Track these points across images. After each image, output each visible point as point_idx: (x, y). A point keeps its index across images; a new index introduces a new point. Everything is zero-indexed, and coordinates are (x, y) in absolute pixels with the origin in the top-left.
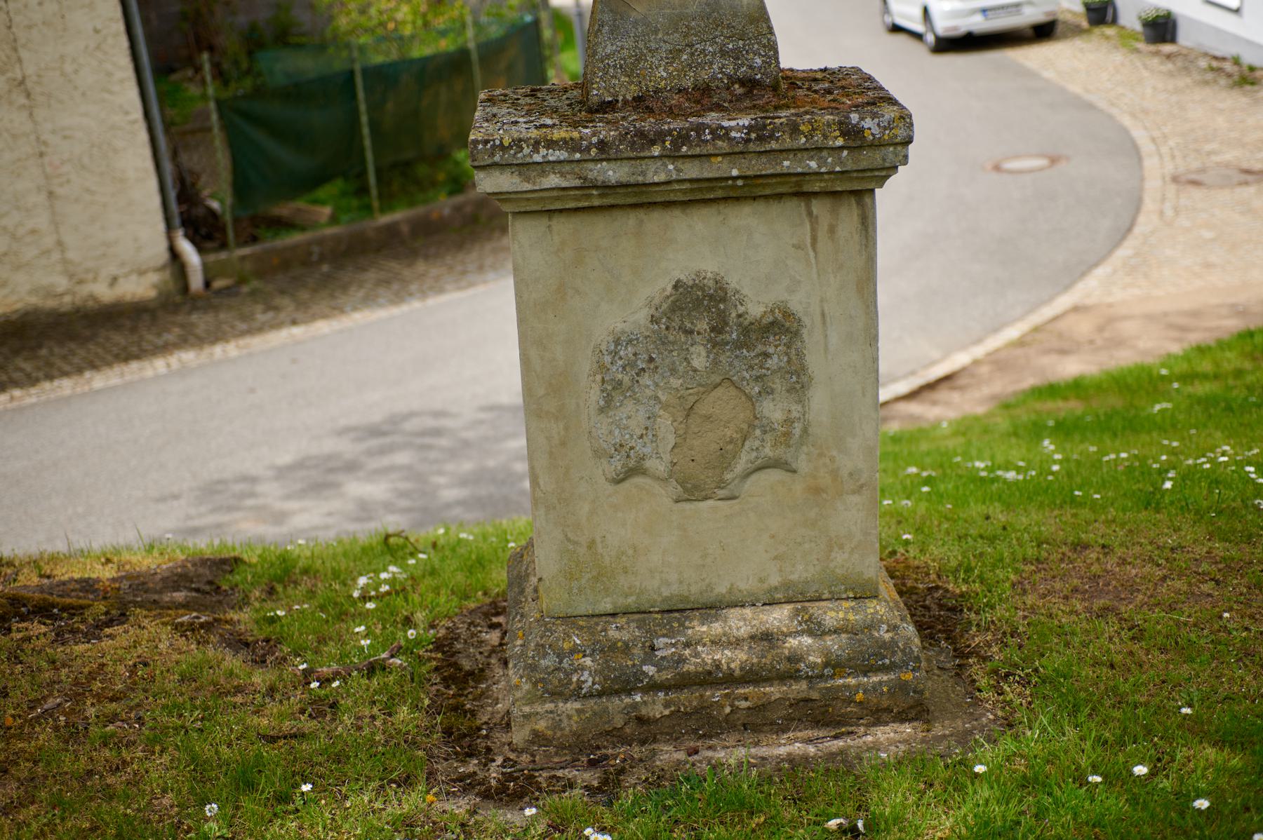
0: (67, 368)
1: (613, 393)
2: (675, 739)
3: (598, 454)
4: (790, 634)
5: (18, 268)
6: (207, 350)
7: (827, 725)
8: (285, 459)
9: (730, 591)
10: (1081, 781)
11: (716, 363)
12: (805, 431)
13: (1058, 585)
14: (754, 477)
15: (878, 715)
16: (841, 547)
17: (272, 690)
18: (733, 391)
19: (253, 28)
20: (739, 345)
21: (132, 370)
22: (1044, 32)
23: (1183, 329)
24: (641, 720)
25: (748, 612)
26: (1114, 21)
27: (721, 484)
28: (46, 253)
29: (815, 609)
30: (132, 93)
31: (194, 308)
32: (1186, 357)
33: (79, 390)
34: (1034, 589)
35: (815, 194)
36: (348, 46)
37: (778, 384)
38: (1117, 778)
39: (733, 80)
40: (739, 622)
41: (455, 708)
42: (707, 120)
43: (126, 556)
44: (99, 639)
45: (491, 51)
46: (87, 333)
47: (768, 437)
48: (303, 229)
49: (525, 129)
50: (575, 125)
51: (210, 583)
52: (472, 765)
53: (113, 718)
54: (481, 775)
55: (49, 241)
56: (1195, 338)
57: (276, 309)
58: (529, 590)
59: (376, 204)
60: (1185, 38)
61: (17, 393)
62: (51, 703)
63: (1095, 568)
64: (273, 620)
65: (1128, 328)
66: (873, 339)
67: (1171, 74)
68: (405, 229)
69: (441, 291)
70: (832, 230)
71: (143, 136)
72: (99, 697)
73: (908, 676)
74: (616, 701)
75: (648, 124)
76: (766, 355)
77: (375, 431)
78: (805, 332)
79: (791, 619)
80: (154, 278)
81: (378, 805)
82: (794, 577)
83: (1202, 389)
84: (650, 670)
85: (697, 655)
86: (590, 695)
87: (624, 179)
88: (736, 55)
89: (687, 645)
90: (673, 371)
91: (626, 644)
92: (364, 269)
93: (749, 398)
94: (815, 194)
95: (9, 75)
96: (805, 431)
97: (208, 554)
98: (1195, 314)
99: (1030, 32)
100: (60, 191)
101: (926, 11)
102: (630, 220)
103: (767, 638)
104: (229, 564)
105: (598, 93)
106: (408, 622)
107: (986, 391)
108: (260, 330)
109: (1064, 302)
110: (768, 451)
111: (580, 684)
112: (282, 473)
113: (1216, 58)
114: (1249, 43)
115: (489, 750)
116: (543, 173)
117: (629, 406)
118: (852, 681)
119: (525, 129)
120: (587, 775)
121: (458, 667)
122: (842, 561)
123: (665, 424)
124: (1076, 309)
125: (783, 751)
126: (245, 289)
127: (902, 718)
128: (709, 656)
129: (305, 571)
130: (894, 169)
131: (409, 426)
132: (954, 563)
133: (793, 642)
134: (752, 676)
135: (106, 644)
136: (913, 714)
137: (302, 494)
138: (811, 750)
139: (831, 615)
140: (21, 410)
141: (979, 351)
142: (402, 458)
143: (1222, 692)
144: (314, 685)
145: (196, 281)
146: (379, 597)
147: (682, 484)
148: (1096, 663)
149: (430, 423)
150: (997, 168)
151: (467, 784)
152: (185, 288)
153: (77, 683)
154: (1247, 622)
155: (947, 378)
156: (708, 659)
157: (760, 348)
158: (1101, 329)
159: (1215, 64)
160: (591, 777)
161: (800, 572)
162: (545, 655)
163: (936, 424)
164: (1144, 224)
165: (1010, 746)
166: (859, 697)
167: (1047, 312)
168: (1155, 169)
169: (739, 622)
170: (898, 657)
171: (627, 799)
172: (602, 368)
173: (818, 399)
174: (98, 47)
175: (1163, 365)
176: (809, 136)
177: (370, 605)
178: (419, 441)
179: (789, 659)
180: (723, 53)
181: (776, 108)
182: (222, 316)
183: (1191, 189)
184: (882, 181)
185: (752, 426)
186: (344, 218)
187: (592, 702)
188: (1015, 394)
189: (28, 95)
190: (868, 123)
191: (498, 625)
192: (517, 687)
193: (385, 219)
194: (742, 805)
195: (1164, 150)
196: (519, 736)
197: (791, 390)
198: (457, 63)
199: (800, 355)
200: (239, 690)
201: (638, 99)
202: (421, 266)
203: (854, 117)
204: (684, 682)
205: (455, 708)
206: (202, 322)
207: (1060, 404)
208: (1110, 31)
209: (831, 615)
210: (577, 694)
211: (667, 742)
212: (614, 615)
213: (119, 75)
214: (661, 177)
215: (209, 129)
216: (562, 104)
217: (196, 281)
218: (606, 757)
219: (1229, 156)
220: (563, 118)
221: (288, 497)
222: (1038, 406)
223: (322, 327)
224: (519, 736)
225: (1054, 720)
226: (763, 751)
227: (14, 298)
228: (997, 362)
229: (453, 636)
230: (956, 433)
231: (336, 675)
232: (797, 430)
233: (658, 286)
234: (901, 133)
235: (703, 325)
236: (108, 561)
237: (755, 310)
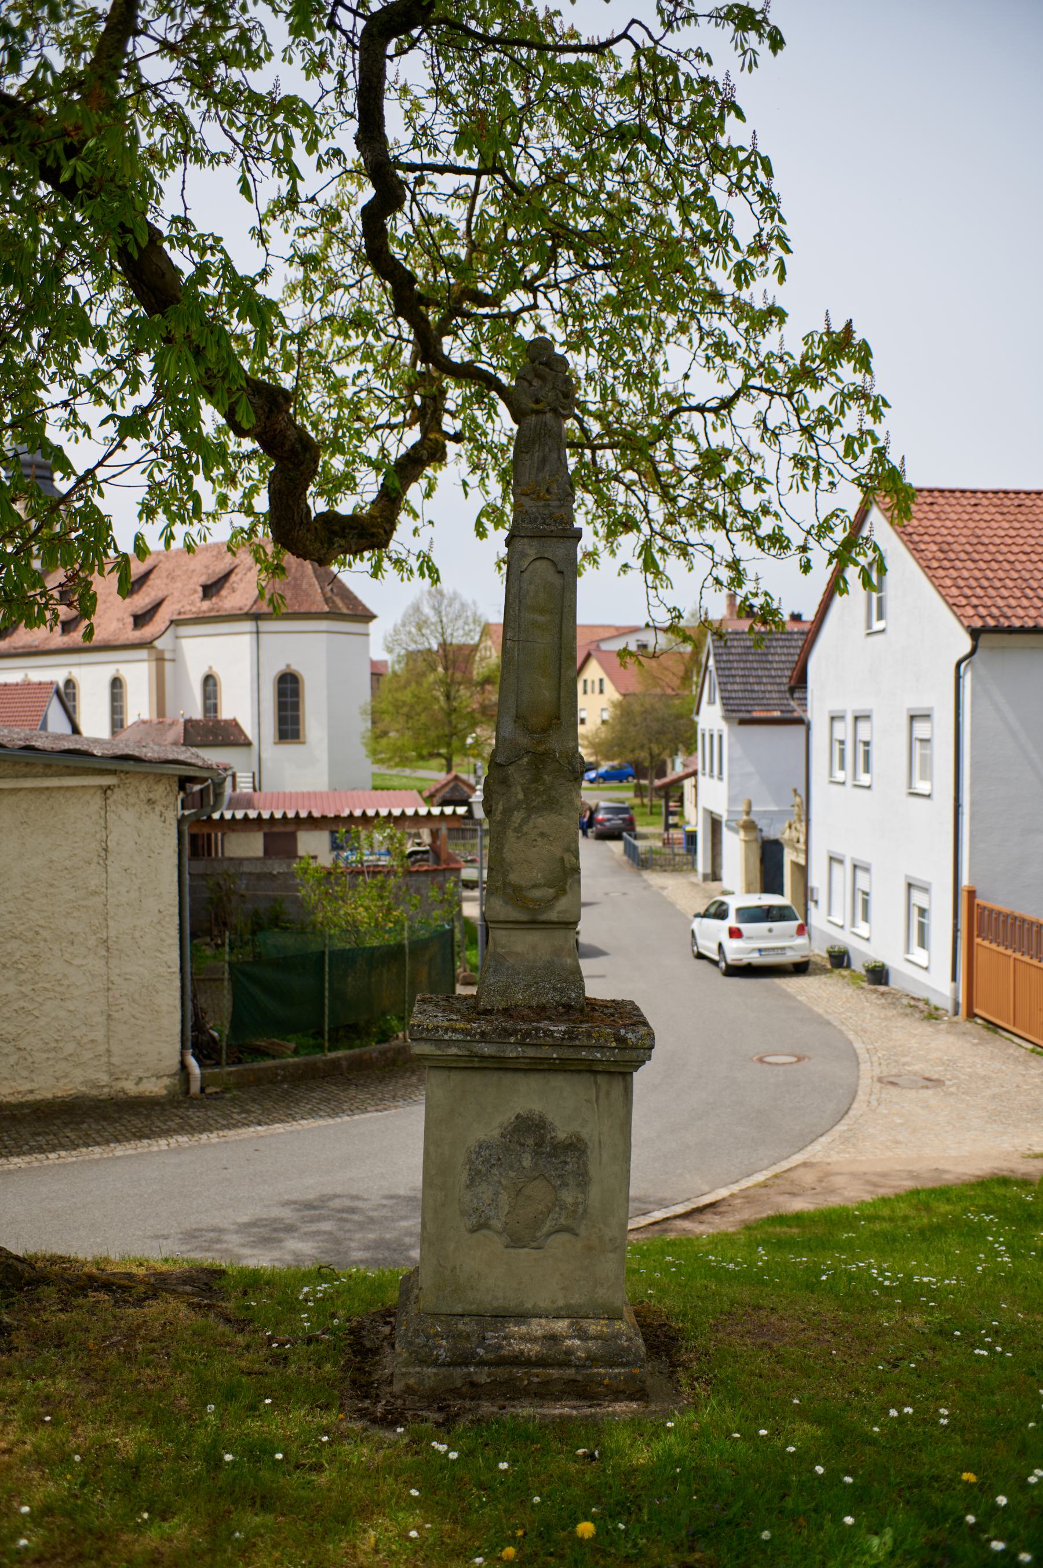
0: (99, 1139)
1: (475, 1177)
2: (492, 1399)
3: (463, 1213)
4: (567, 1337)
5: (77, 1065)
6: (197, 1137)
7: (585, 1398)
8: (245, 1219)
9: (534, 1307)
10: (728, 1435)
11: (536, 1164)
12: (585, 1210)
13: (739, 1328)
14: (553, 1237)
15: (617, 1395)
16: (602, 1285)
17: (248, 1347)
18: (545, 1183)
19: (256, 913)
20: (550, 1155)
21: (144, 1146)
22: (800, 969)
23: (876, 1185)
24: (473, 1384)
25: (543, 1321)
26: (848, 966)
27: (534, 1239)
28: (98, 1057)
29: (584, 1323)
30: (175, 954)
31: (192, 1106)
32: (873, 1205)
33: (105, 1156)
34: (724, 1327)
35: (599, 1072)
36: (322, 934)
37: (571, 1181)
38: (750, 1437)
39: (559, 1004)
40: (537, 1327)
41: (359, 1369)
42: (542, 1025)
43: (152, 1263)
44: (142, 1307)
45: (419, 947)
46: (116, 1115)
47: (563, 1212)
48: (274, 1057)
49: (441, 1021)
50: (469, 1021)
51: (206, 1284)
52: (367, 1403)
53: (153, 1351)
54: (371, 1409)
55: (102, 1049)
56: (882, 1192)
57: (248, 1112)
58: (412, 1297)
59: (327, 1045)
60: (894, 982)
61: (63, 1153)
62: (115, 1339)
63: (764, 1321)
64: (248, 1308)
65: (839, 1181)
66: (627, 1159)
67: (883, 1007)
68: (344, 1063)
69: (365, 1111)
70: (608, 1093)
71: (177, 983)
72: (144, 1339)
73: (637, 1371)
74: (458, 1370)
75: (508, 1025)
76: (566, 1163)
77: (309, 1206)
78: (589, 1151)
79: (569, 1327)
80: (166, 1081)
81: (309, 1418)
82: (573, 1302)
83: (877, 1227)
84: (481, 1351)
85: (510, 1345)
86: (443, 1365)
87: (493, 1054)
88: (562, 991)
89: (505, 1338)
90: (511, 1167)
91: (468, 1334)
92: (312, 1090)
93: (554, 1187)
94: (599, 1072)
96: (585, 1210)
97: (205, 1265)
98: (884, 1175)
99: (791, 968)
100: (115, 1015)
101: (720, 946)
102: (495, 1076)
103: (553, 1338)
104: (219, 1273)
105: (483, 1004)
106: (333, 1316)
107: (738, 1217)
108: (235, 1126)
109: (797, 1159)
110: (563, 1221)
111: (438, 1355)
112: (243, 1228)
113: (913, 998)
114: (935, 991)
115: (378, 1395)
116: (449, 1046)
117: (484, 1186)
118: (602, 1370)
119: (441, 1021)
120: (436, 1416)
121: (363, 1346)
122: (602, 1294)
123: (504, 1197)
124: (805, 1164)
125: (557, 1412)
126: (228, 1096)
127: (631, 1398)
128: (517, 1346)
129: (267, 1283)
130: (643, 1062)
131: (336, 1203)
132: (677, 1310)
133: (569, 1342)
134: (541, 1362)
135: (146, 1310)
136: (638, 1396)
137: (253, 1245)
138: (575, 1412)
139: (593, 1327)
140: (64, 1165)
141: (735, 1188)
142: (326, 1226)
143: (822, 1395)
144: (275, 1345)
146: (316, 1300)
147: (510, 1236)
148: (752, 1374)
149: (348, 1203)
150: (761, 1060)
151: (363, 1414)
152: (187, 1091)
153: (130, 1329)
154: (846, 1358)
155: (712, 1205)
156: (517, 1348)
157: (562, 1158)
158: (820, 1181)
159: (912, 1003)
160: (439, 1417)
161: (576, 1299)
162: (418, 1337)
163: (698, 1237)
164: (858, 1108)
165: (692, 1416)
166: (606, 1381)
167: (785, 1165)
168: (867, 1072)
169: (537, 1327)
170: (631, 1358)
171: (460, 1427)
172: (470, 1161)
173: (595, 1192)
175: (857, 1209)
176: (598, 1040)
177: (311, 1304)
178: (339, 1215)
179: (565, 1353)
180: (555, 989)
181: (581, 1022)
182: (210, 1114)
183: (889, 1087)
184: (636, 1068)
185: (554, 1205)
186: (302, 1052)
187: (443, 1369)
188: (756, 1221)
189: (108, 950)
190: (630, 1035)
191: (390, 1323)
192: (400, 1354)
193: (332, 1055)
194: (528, 1438)
195: (875, 1059)
196: (397, 1387)
197: (578, 1185)
198: (394, 954)
199: (585, 1165)
200: (228, 1344)
201: (506, 1010)
202: (352, 1092)
203: (623, 1032)
204: (501, 1362)
205: (359, 1369)
206: (195, 1115)
207: (785, 1229)
208: (845, 972)
209: (593, 1327)
210: (435, 1363)
211: (487, 1400)
212: (462, 1316)
213: (169, 941)
214: (514, 1055)
215: (222, 980)
216: (462, 1007)
218: (449, 1406)
219: (917, 1067)
220: (463, 1016)
221: (243, 1245)
222: (770, 1230)
223: (278, 1128)
224: (397, 1387)
225: (720, 1404)
226: (545, 1411)
227: (71, 1086)
228: (748, 1197)
229: (361, 1327)
230: (710, 1243)
231: (288, 1341)
232: (580, 1210)
233: (506, 1116)
234: (647, 1043)
235: (530, 1142)
236: (141, 1264)
237: (562, 1136)
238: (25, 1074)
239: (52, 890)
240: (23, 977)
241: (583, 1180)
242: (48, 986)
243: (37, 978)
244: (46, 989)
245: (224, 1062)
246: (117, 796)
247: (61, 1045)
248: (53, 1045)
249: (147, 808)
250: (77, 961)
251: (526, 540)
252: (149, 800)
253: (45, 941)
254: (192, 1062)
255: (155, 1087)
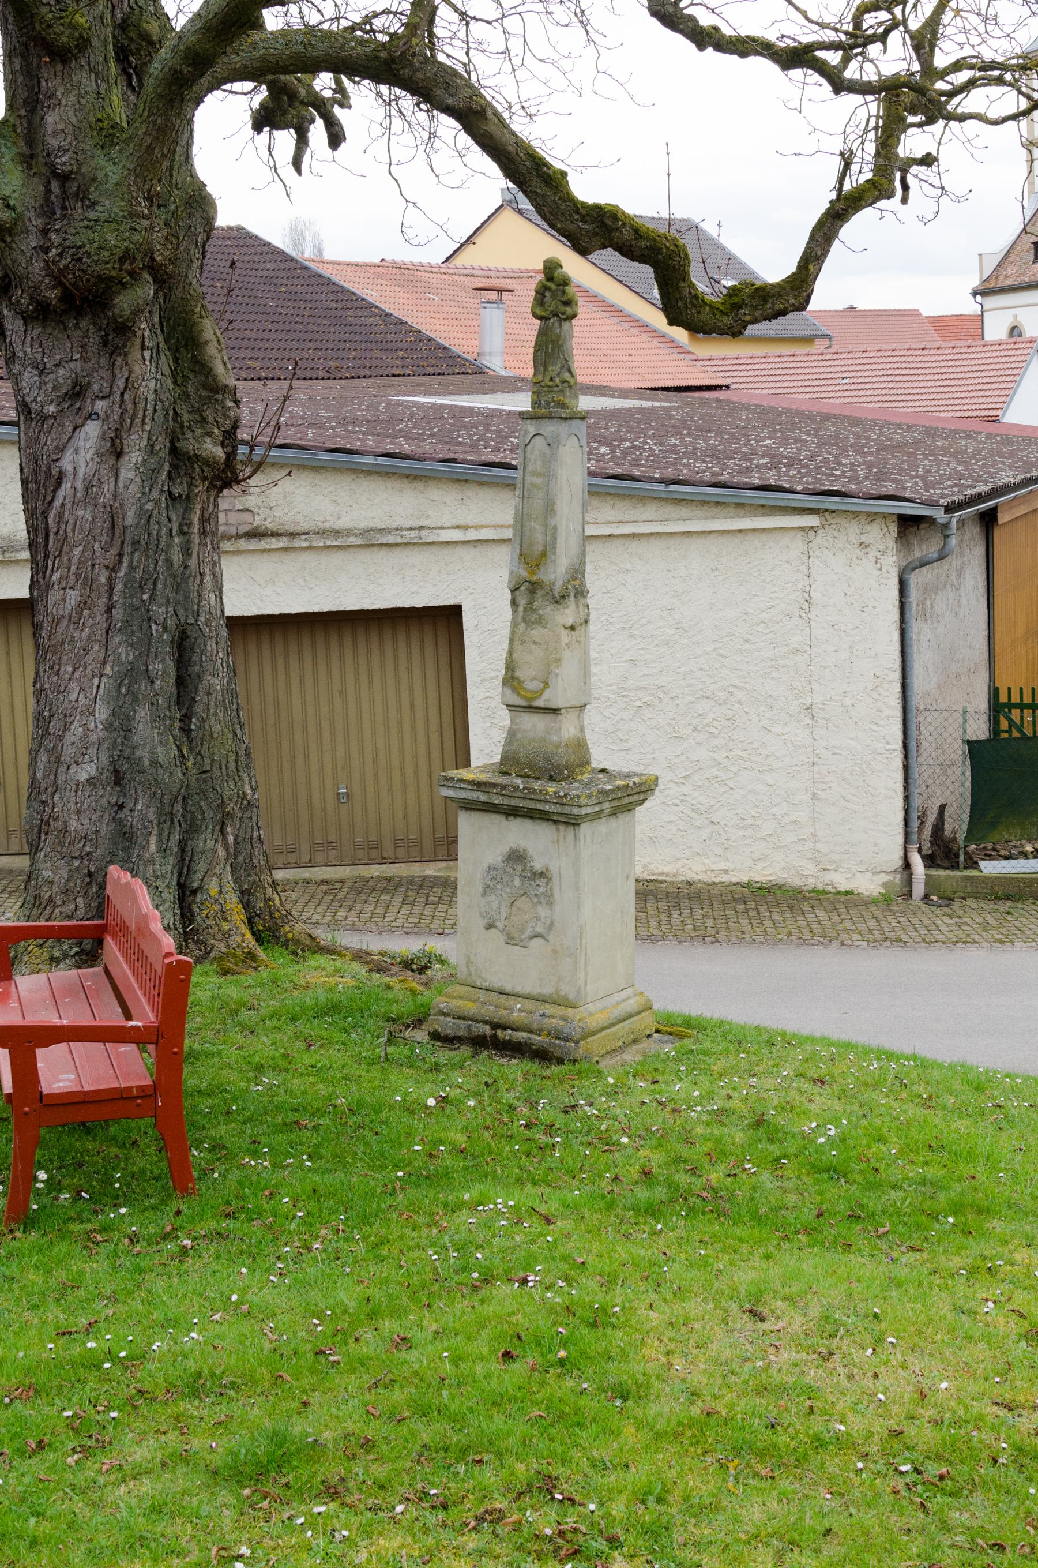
1: (487, 890)
70: (565, 837)
76: (538, 885)
80: (884, 878)
95: (802, 701)
145: (919, 889)
157: (538, 882)
174: (874, 689)
213: (887, 712)
217: (919, 889)
233: (504, 849)
238: (719, 851)
239: (746, 646)
240: (716, 742)
241: (549, 900)
242: (744, 754)
243: (731, 744)
244: (741, 758)
245: (961, 866)
246: (819, 539)
247: (759, 822)
248: (750, 822)
249: (859, 553)
250: (777, 729)
251: (529, 421)
252: (861, 544)
253: (740, 703)
254: (916, 860)
255: (870, 886)
